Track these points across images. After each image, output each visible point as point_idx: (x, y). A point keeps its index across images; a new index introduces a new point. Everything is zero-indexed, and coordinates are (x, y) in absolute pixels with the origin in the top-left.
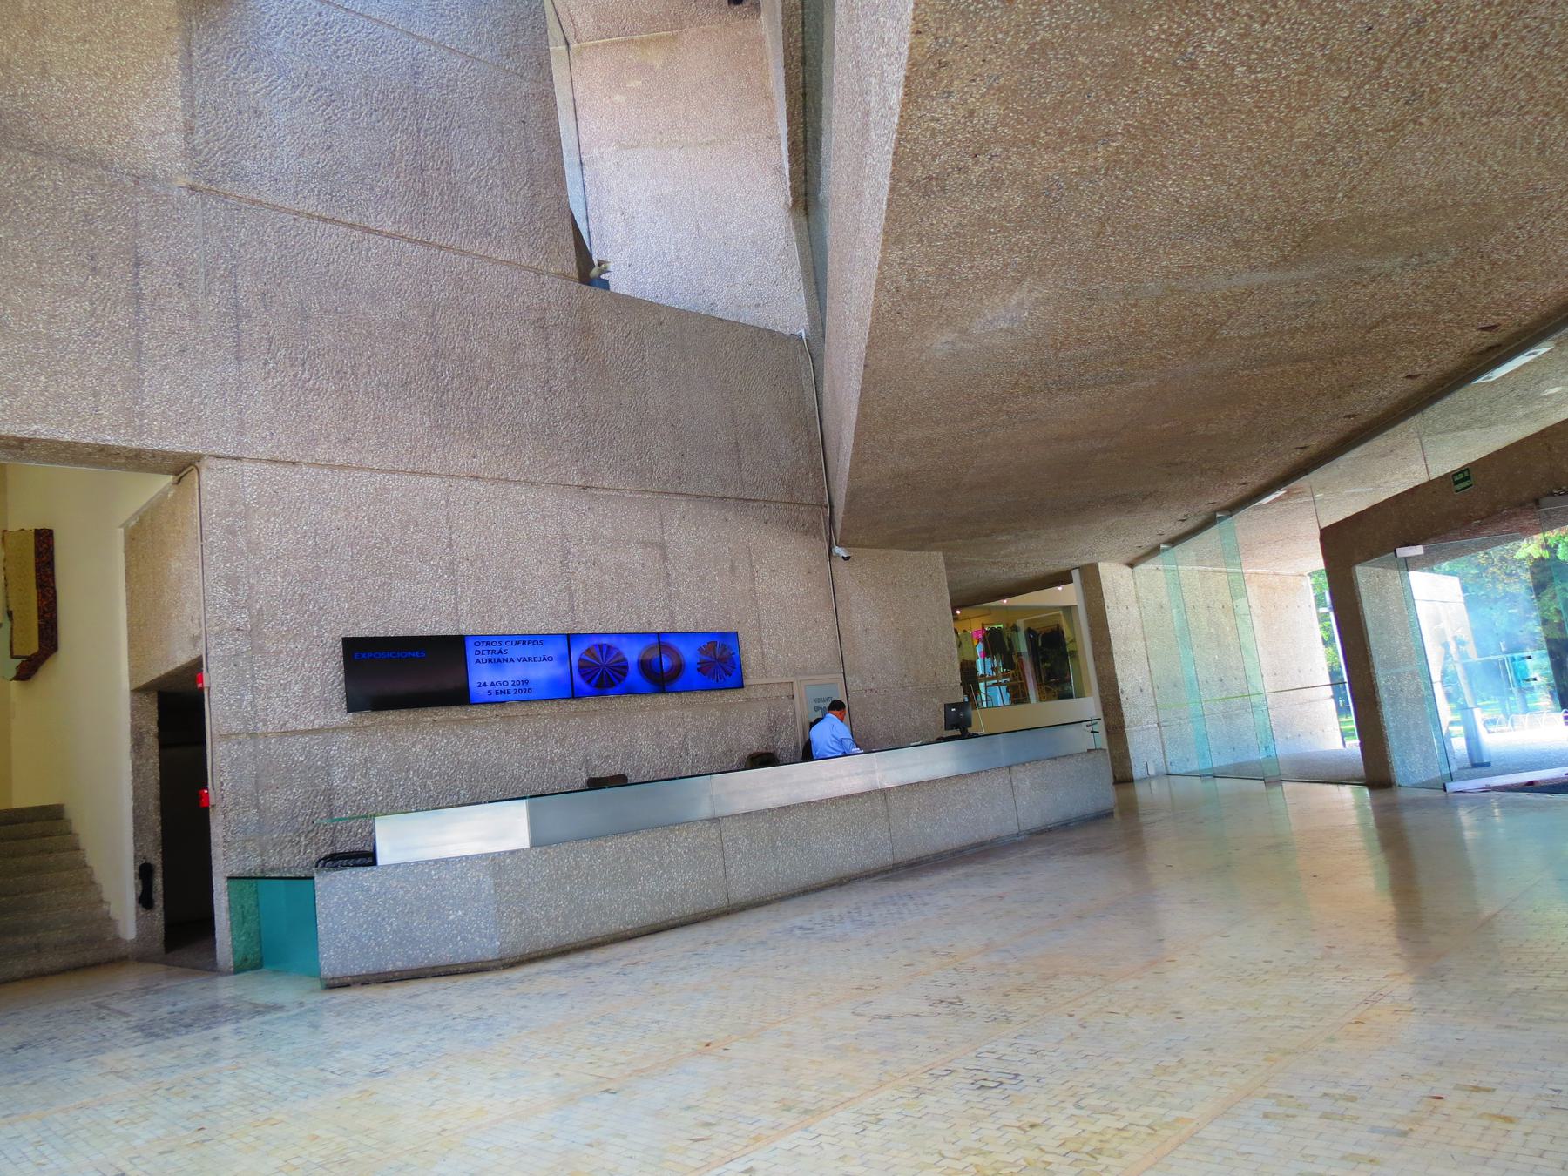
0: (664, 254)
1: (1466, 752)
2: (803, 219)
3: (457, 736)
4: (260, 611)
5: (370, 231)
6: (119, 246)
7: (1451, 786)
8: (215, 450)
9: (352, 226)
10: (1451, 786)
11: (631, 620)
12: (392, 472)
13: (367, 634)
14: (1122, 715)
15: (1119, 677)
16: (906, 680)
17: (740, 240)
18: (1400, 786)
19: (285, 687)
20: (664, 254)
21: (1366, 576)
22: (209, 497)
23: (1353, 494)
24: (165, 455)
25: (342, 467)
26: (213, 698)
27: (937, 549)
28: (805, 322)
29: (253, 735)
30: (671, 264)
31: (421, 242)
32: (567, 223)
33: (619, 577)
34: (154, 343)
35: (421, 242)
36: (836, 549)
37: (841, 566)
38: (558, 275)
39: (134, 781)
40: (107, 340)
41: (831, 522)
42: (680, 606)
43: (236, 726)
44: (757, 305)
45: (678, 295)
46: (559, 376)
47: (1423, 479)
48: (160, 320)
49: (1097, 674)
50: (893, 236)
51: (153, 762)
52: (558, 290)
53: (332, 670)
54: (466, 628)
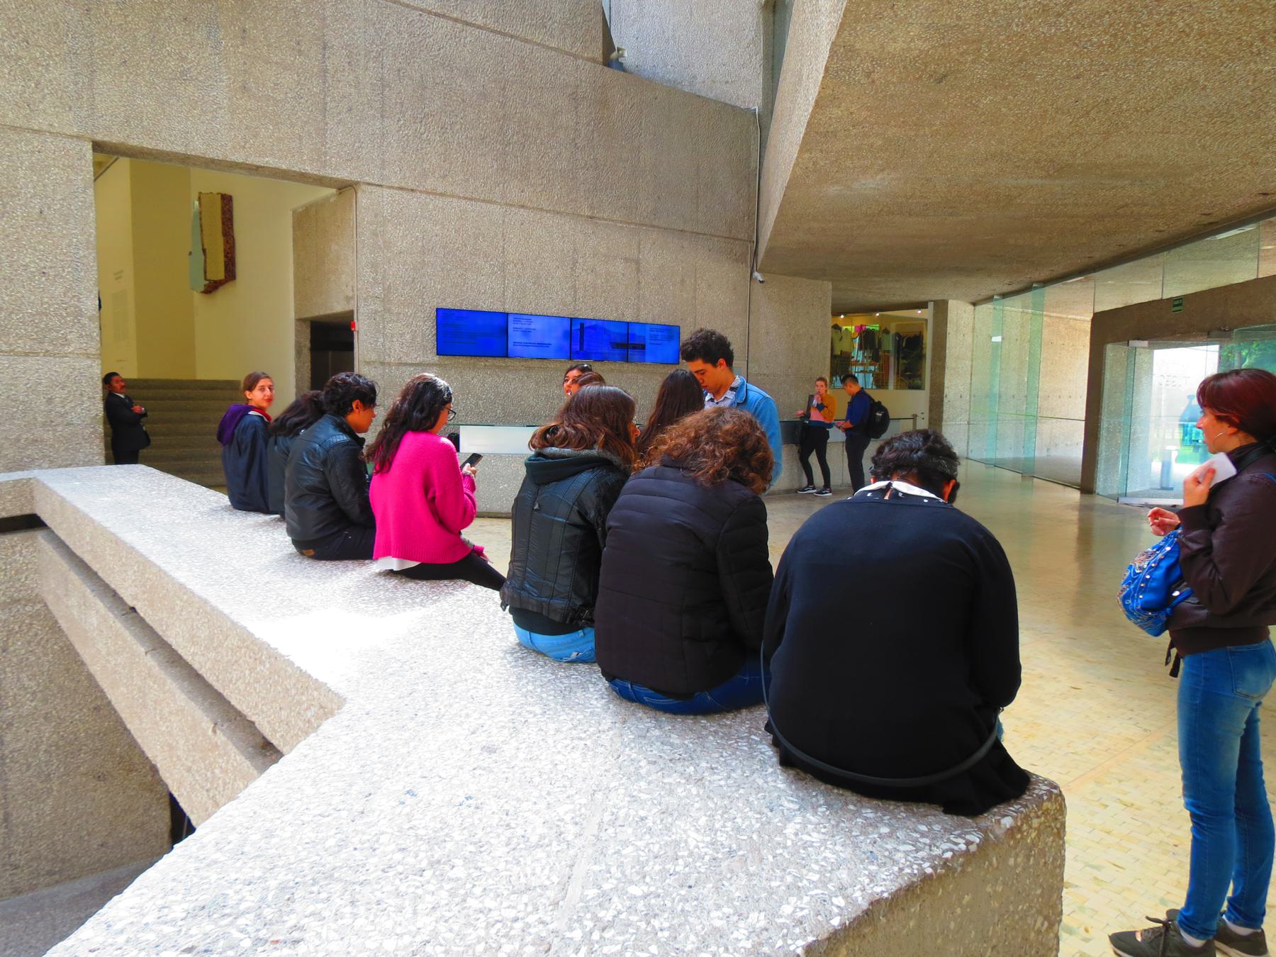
0: (664, 32)
1: (1159, 477)
2: (771, 15)
3: (498, 376)
4: (390, 286)
5: (467, 24)
6: (314, 34)
7: (1122, 500)
8: (367, 179)
9: (456, 20)
10: (1122, 500)
11: (612, 311)
12: (471, 199)
13: (450, 306)
14: (942, 412)
15: (946, 385)
16: (790, 371)
17: (721, 28)
18: (1098, 494)
19: (402, 335)
20: (664, 32)
21: (1113, 352)
22: (363, 211)
23: (1137, 284)
24: (336, 180)
25: (442, 195)
26: (361, 338)
27: (829, 280)
28: (759, 100)
29: (382, 363)
30: (667, 41)
31: (500, 33)
32: (600, 18)
33: (607, 281)
34: (334, 104)
35: (500, 33)
36: (756, 274)
37: (757, 286)
38: (588, 59)
39: (296, 376)
40: (307, 101)
41: (756, 253)
42: (644, 305)
43: (374, 357)
44: (727, 82)
45: (669, 67)
46: (583, 135)
47: (1158, 297)
48: (338, 88)
49: (931, 380)
50: (806, 146)
51: (308, 364)
52: (586, 72)
53: (428, 330)
54: (508, 308)
